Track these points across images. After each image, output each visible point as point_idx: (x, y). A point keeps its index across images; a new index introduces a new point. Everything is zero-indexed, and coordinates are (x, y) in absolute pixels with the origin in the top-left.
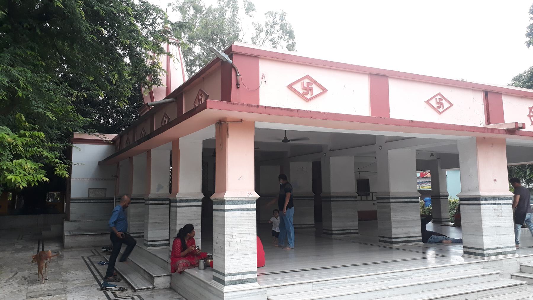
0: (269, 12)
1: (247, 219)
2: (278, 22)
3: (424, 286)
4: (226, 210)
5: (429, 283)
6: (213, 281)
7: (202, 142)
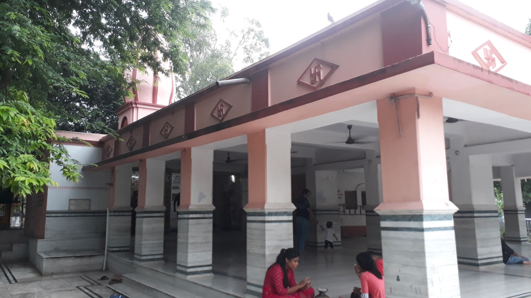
4: (425, 230)
7: (290, 136)
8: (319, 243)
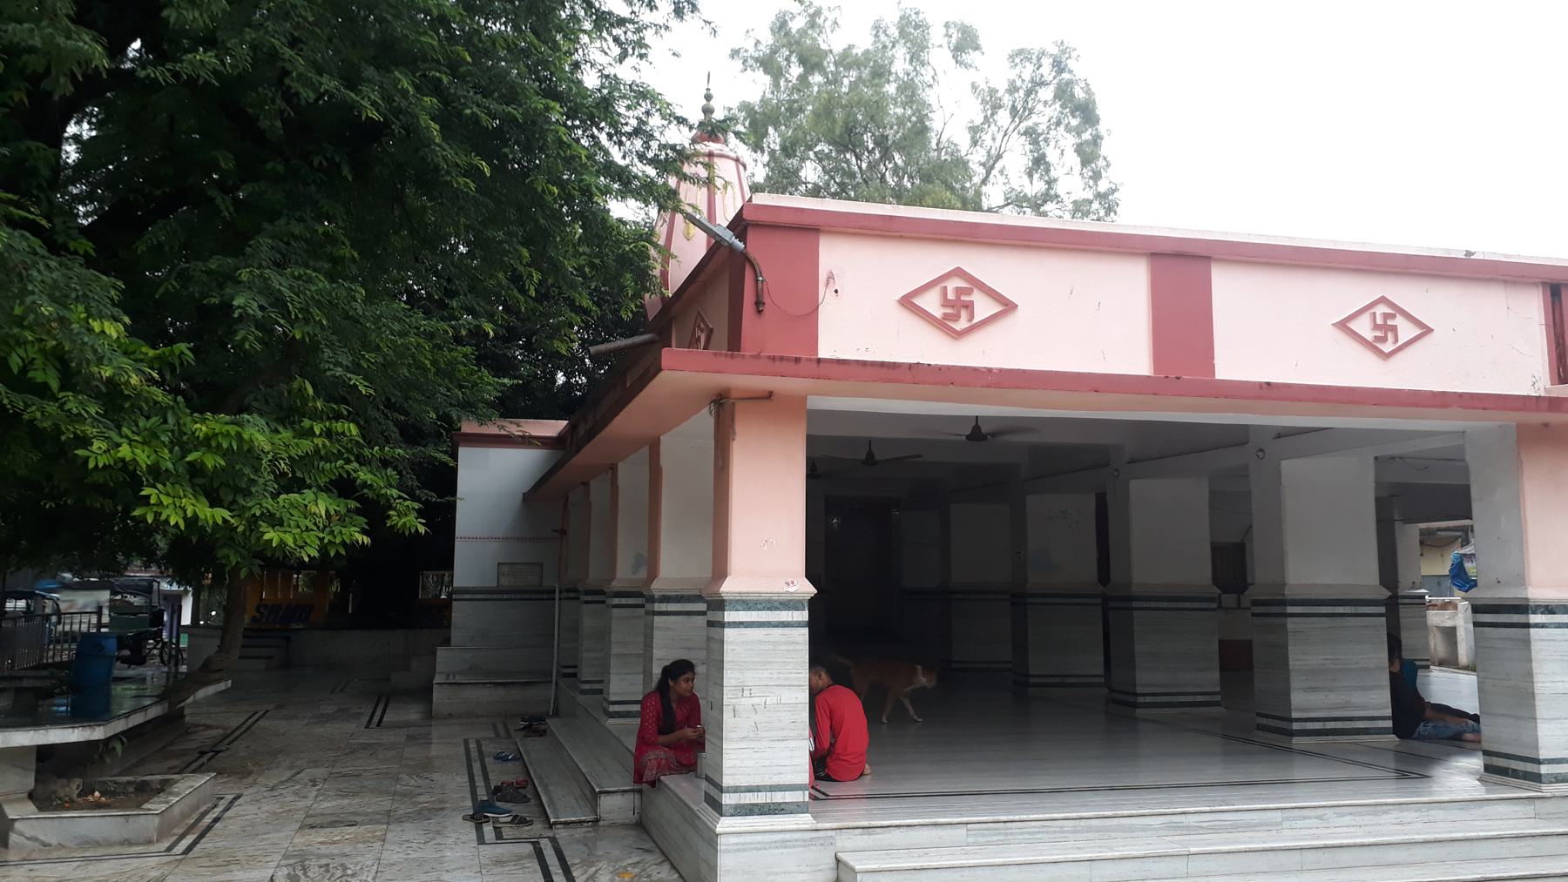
0: (1021, 52)
1: (784, 647)
2: (1048, 78)
3: (1307, 854)
4: (726, 625)
5: (1326, 847)
6: (705, 804)
8: (1034, 676)
